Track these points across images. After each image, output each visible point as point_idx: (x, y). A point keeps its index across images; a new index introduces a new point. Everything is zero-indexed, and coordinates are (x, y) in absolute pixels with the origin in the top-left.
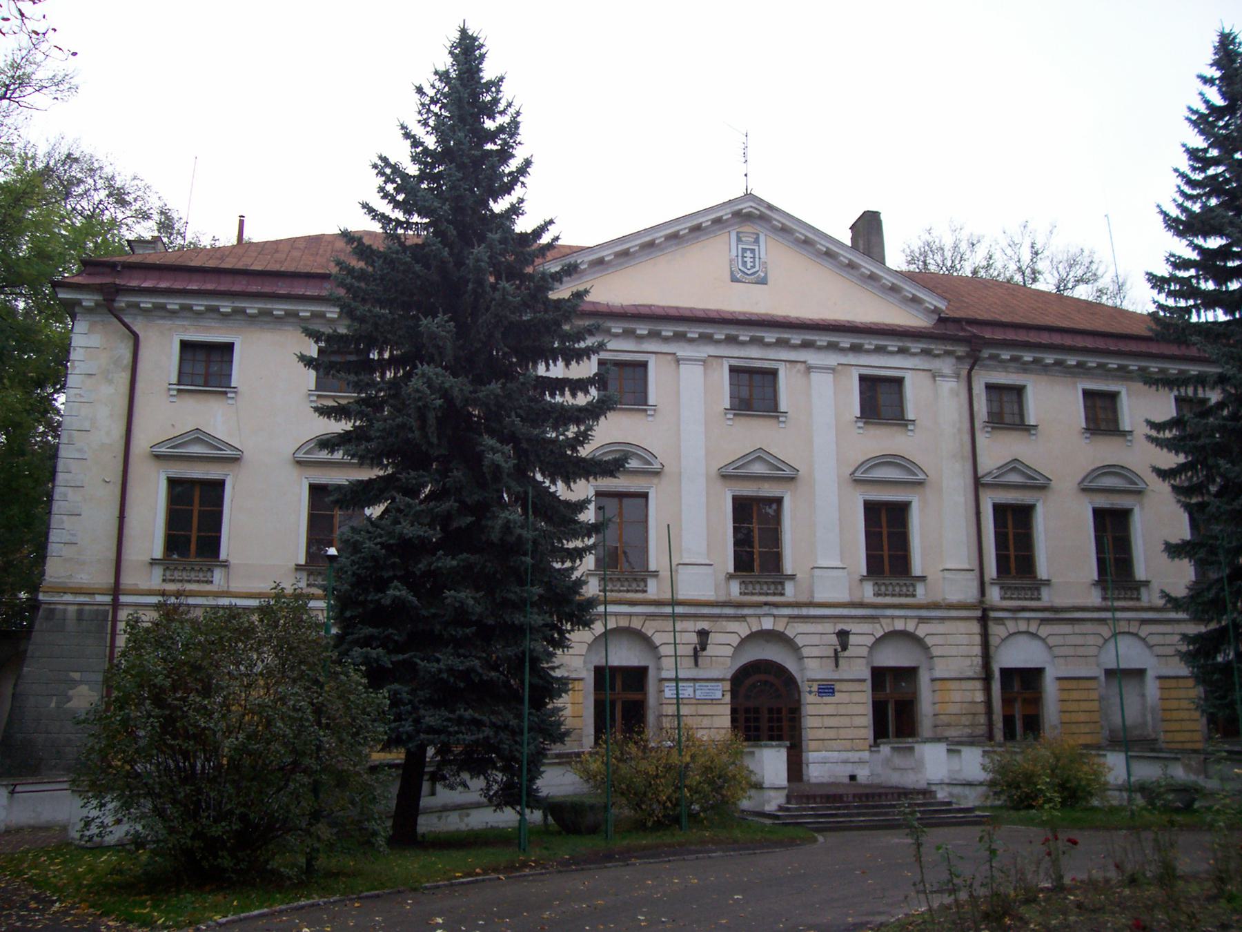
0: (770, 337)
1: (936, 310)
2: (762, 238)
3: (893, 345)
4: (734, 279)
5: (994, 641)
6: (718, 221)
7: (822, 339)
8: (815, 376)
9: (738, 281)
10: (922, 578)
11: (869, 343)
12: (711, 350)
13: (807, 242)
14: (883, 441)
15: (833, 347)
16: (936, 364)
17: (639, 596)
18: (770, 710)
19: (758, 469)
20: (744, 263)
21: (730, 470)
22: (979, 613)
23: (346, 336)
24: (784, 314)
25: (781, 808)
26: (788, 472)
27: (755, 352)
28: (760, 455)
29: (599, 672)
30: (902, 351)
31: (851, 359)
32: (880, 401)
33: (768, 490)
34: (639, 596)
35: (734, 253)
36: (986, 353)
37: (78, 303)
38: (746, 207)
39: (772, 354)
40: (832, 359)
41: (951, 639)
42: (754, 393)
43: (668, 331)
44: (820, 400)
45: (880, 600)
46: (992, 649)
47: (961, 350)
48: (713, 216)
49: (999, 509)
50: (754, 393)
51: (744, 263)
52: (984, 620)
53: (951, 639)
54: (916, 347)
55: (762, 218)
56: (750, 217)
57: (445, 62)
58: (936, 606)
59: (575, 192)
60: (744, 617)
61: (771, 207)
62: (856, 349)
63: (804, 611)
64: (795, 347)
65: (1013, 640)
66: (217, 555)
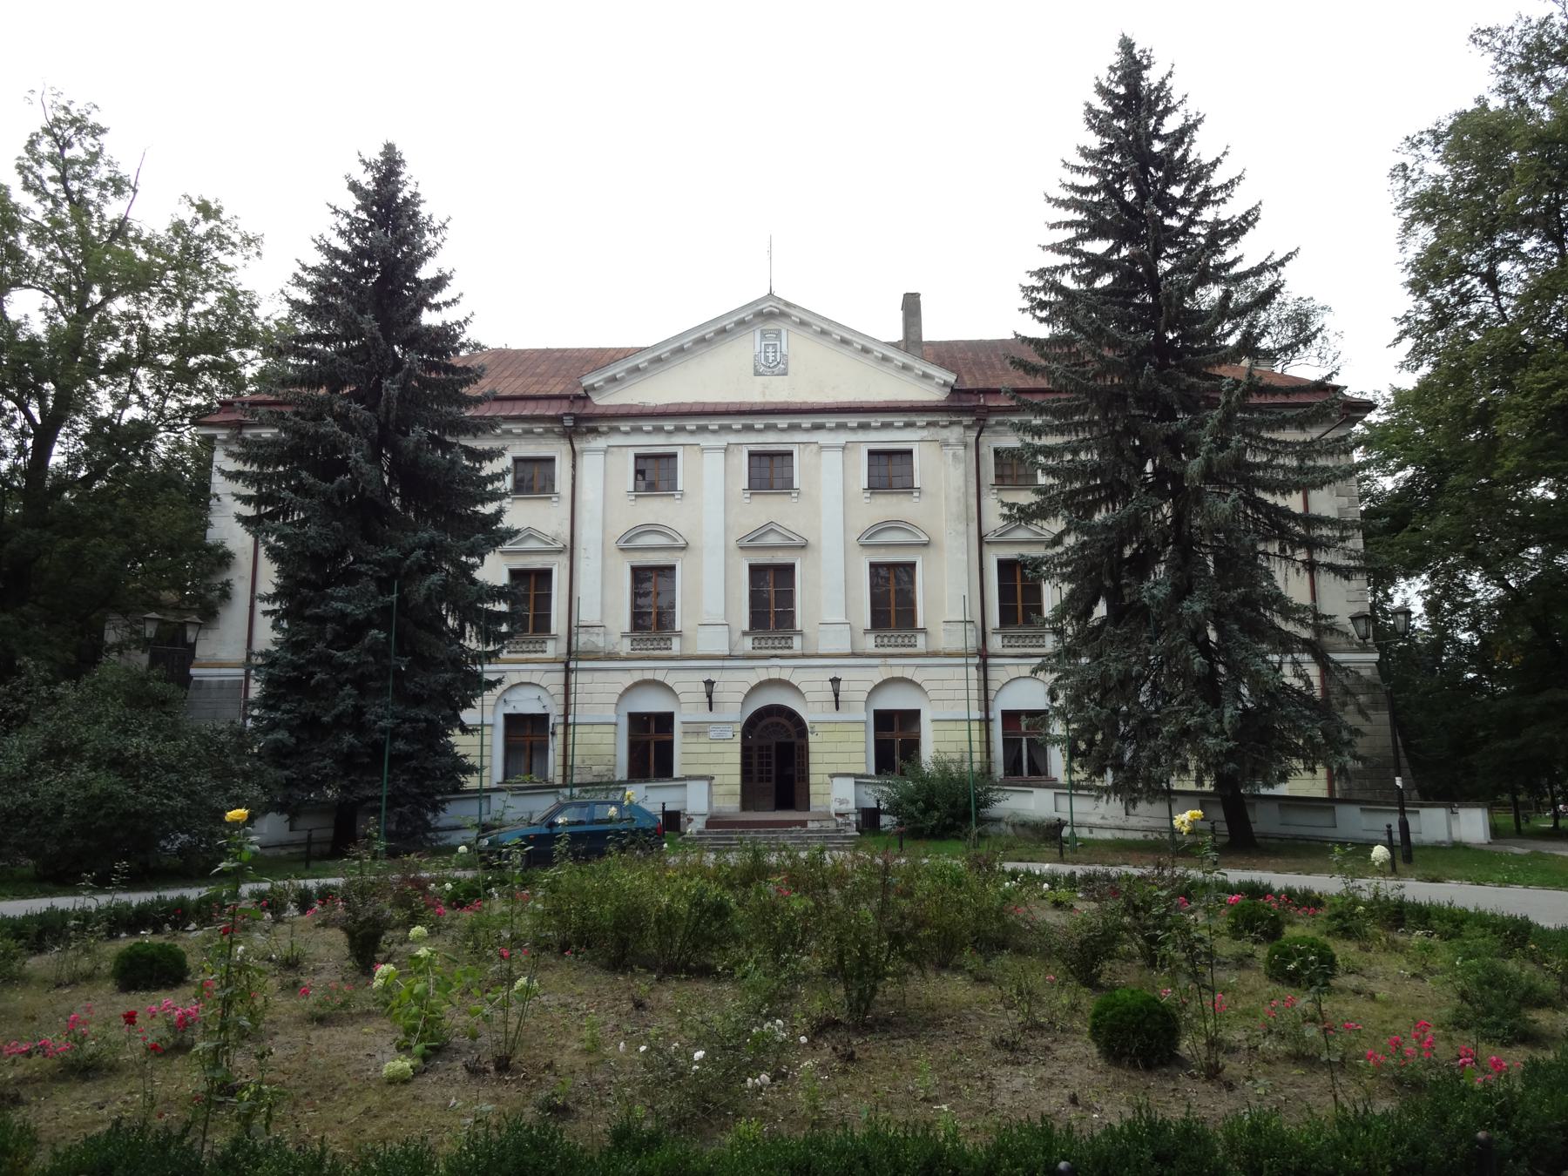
0: (782, 422)
1: (946, 384)
2: (784, 333)
3: (899, 420)
4: (757, 373)
5: (994, 686)
6: (741, 323)
7: (830, 421)
8: (826, 455)
9: (761, 374)
10: (923, 630)
11: (876, 421)
12: (733, 439)
13: (824, 333)
14: (890, 506)
15: (841, 427)
16: (945, 434)
17: (665, 653)
18: (761, 748)
19: (772, 539)
20: (767, 358)
21: (745, 543)
22: (977, 660)
23: (1409, 488)
24: (782, 399)
25: (699, 832)
26: (798, 541)
27: (771, 437)
28: (769, 529)
29: (508, 717)
30: (908, 425)
31: (861, 436)
32: (889, 472)
33: (781, 558)
34: (665, 653)
35: (758, 349)
36: (992, 420)
37: (213, 437)
38: (767, 307)
39: (786, 438)
40: (842, 438)
41: (947, 685)
42: (770, 471)
43: (691, 424)
44: (830, 472)
45: (758, 652)
46: (992, 695)
47: (967, 420)
48: (825, 327)
49: (1006, 567)
50: (770, 471)
51: (767, 358)
52: (984, 667)
53: (947, 685)
54: (921, 420)
55: (783, 314)
56: (769, 315)
57: (352, 195)
58: (935, 655)
59: (496, 296)
60: (629, 670)
61: (788, 304)
62: (864, 427)
63: (727, 663)
64: (760, 431)
65: (1006, 689)
66: (792, 625)
